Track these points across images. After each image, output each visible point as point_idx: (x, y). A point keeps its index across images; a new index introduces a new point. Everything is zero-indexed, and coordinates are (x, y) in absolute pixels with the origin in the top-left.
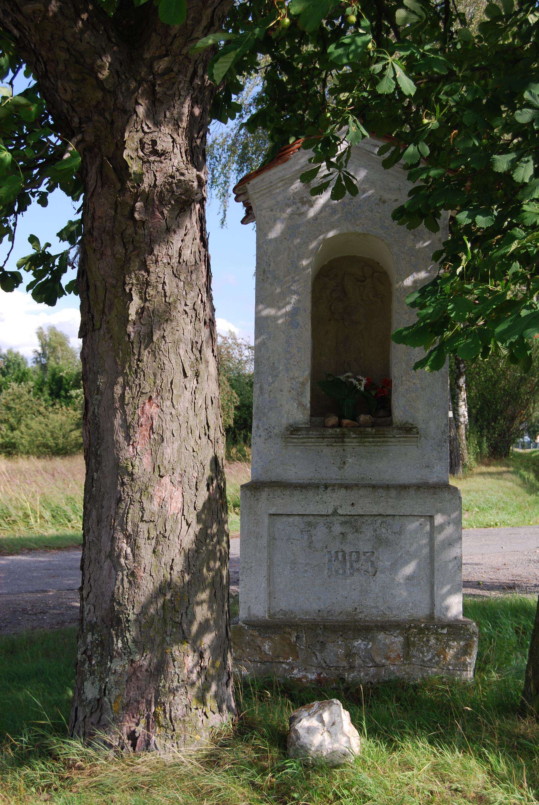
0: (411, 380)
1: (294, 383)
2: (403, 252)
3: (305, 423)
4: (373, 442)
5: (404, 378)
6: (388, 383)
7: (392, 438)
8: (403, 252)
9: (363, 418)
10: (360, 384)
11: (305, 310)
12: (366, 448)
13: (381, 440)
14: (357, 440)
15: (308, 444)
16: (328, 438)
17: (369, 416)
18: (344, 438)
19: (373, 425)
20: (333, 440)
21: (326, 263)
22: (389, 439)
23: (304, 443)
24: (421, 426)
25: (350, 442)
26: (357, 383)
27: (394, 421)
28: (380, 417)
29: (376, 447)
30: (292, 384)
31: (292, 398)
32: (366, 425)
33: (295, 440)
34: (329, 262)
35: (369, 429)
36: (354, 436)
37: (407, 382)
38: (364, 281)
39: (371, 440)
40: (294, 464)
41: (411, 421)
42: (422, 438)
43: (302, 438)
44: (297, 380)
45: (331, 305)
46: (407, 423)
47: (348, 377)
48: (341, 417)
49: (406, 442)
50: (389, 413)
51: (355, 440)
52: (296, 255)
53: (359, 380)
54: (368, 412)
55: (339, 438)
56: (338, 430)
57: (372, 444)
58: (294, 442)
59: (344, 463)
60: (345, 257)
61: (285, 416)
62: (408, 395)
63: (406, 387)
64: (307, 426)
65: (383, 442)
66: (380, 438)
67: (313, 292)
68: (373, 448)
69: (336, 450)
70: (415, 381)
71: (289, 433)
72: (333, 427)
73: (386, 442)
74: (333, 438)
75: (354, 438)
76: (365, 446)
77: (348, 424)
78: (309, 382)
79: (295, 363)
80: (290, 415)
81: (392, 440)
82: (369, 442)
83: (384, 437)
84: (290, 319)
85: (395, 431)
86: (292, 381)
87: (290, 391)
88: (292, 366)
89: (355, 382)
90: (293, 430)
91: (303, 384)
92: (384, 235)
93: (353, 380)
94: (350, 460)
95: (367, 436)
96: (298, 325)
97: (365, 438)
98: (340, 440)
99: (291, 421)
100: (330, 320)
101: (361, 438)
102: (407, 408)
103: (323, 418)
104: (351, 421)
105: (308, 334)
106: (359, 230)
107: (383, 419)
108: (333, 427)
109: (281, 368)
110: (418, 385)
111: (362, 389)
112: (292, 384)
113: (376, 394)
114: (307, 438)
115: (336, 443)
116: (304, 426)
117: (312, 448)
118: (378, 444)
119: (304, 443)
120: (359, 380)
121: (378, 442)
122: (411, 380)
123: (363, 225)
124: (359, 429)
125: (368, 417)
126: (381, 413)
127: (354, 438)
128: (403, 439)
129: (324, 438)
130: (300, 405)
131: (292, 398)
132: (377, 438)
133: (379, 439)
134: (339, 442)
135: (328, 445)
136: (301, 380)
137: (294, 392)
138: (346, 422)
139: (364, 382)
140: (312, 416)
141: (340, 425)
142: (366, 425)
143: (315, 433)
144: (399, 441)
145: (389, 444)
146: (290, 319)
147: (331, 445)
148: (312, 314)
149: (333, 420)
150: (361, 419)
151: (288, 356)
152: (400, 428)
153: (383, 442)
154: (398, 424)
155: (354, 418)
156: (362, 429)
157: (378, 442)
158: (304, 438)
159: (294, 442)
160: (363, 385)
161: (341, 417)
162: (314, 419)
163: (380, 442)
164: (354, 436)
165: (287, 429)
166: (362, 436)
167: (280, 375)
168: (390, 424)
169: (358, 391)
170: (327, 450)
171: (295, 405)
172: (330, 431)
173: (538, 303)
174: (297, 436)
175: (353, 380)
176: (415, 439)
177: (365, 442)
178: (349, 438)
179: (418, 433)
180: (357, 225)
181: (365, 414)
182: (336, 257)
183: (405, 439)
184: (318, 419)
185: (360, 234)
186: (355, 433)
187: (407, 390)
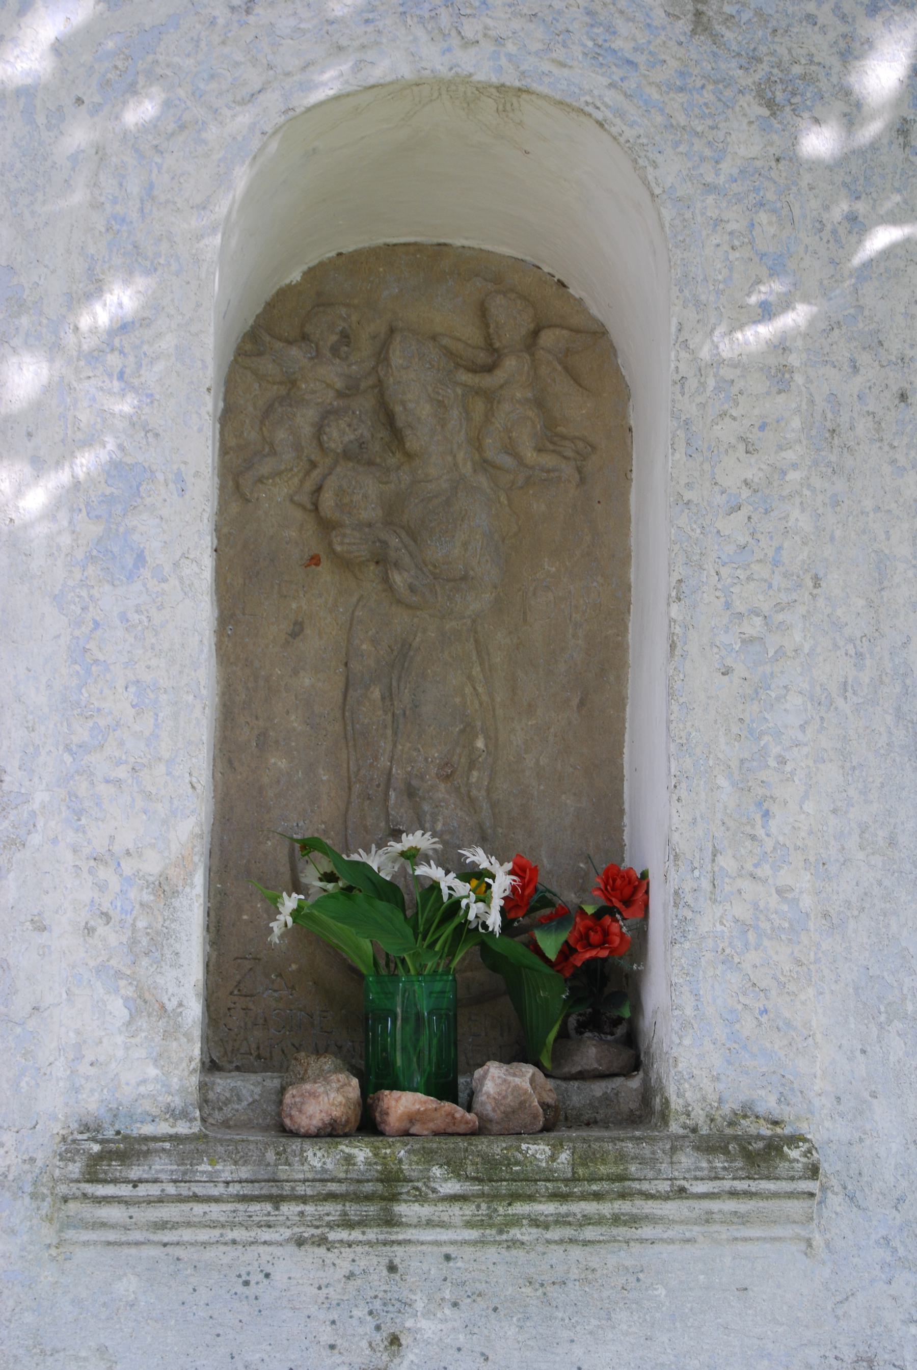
0: (765, 870)
1: (115, 884)
2: (709, 188)
3: (174, 1114)
4: (561, 1221)
5: (726, 862)
6: (627, 892)
7: (666, 1197)
8: (709, 188)
9: (499, 1082)
10: (484, 897)
11: (180, 478)
12: (518, 1254)
13: (606, 1208)
14: (469, 1210)
15: (187, 1235)
16: (303, 1199)
17: (529, 1070)
18: (394, 1198)
19: (553, 1121)
20: (333, 1210)
21: (295, 276)
22: (649, 1207)
23: (162, 1225)
24: (824, 1129)
25: (430, 1224)
26: (462, 889)
27: (676, 1103)
28: (582, 1076)
29: (576, 1252)
30: (102, 887)
31: (101, 970)
32: (514, 1125)
33: (114, 1213)
34: (310, 274)
35: (538, 1150)
36: (452, 1187)
37: (745, 884)
38: (489, 369)
39: (548, 1208)
40: (102, 1350)
41: (768, 1103)
42: (835, 1201)
43: (150, 1201)
44: (128, 867)
45: (319, 489)
46: (746, 1111)
47: (412, 856)
48: (376, 1077)
49: (743, 1219)
50: (631, 1050)
51: (456, 1212)
52: (134, 187)
53: (477, 877)
54: (520, 1052)
55: (369, 1198)
56: (361, 1152)
57: (555, 1234)
58: (103, 1225)
59: (395, 1340)
60: (389, 253)
61: (60, 1069)
62: (752, 957)
63: (740, 910)
64: (183, 1128)
65: (616, 1220)
66: (598, 1197)
67: (228, 417)
68: (556, 1254)
69: (345, 1267)
70: (785, 878)
71: (75, 1169)
72: (330, 1132)
73: (634, 1220)
74: (332, 1197)
75: (454, 1198)
76: (514, 1244)
77: (412, 1118)
78: (199, 879)
79: (122, 772)
80: (84, 1068)
81: (669, 1208)
82: (535, 1222)
83: (623, 1196)
84: (97, 529)
85: (687, 1159)
86: (103, 873)
87: (89, 930)
88: (103, 789)
89: (448, 882)
90: (107, 1155)
91: (164, 889)
92: (611, 97)
93: (435, 872)
94: (428, 1327)
95: (525, 1185)
96: (140, 559)
97: (515, 1197)
98: (372, 1209)
99: (92, 1103)
100: (315, 560)
101: (494, 1197)
102: (747, 1026)
103: (273, 1082)
104: (431, 1102)
105: (193, 612)
106: (479, 66)
107: (599, 1088)
108: (330, 1132)
109: (40, 797)
110: (807, 902)
111: (494, 921)
112: (102, 887)
113: (567, 951)
114: (180, 1199)
115: (349, 1225)
116: (163, 1128)
117: (211, 1254)
118: (590, 1233)
119: (162, 1225)
120: (477, 877)
121: (587, 1221)
122: (765, 870)
123: (499, 41)
124: (482, 1144)
125: (524, 1077)
126: (590, 1053)
127: (454, 1198)
128: (730, 1205)
129: (277, 1200)
130: (147, 1005)
131: (101, 970)
132: (583, 1197)
133: (590, 1207)
134: (362, 1223)
135: (300, 1242)
136: (152, 865)
137: (111, 936)
138: (401, 1104)
139: (502, 883)
140: (211, 1067)
141: (367, 1123)
142: (514, 1125)
143: (226, 1171)
144: (708, 1219)
145: (647, 1231)
146: (97, 529)
147: (322, 1241)
148: (217, 530)
149: (329, 1095)
150: (489, 1087)
151: (82, 733)
152: (712, 1145)
153: (616, 1220)
154: (699, 1116)
155: (444, 1087)
156: (497, 1147)
157: (587, 1221)
158: (160, 1200)
159: (103, 1225)
160: (497, 902)
161: (376, 1077)
162: (223, 1084)
163: (599, 1221)
164: (452, 1187)
165: (69, 1149)
166: (500, 1188)
167: (35, 839)
168: (646, 1112)
169: (468, 933)
170: (296, 1272)
171: (118, 1009)
172: (318, 1158)
173: (1, 1178)
174: (124, 1190)
175: (435, 872)
176: (795, 1207)
177: (515, 1221)
178: (421, 1198)
179: (814, 1171)
180: (468, 44)
181: (507, 1059)
182: (349, 247)
183: (743, 1206)
184: (246, 1088)
185: (482, 89)
186: (456, 1169)
187: (744, 927)
